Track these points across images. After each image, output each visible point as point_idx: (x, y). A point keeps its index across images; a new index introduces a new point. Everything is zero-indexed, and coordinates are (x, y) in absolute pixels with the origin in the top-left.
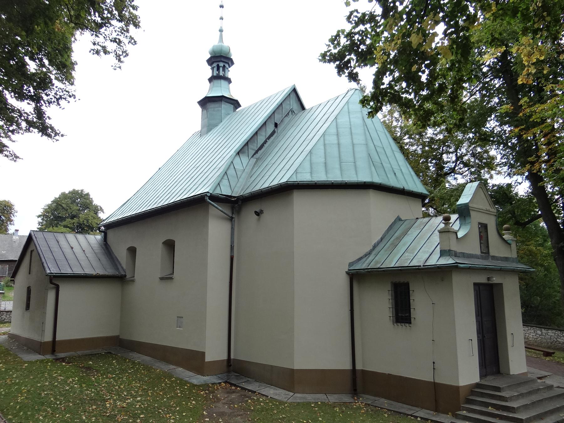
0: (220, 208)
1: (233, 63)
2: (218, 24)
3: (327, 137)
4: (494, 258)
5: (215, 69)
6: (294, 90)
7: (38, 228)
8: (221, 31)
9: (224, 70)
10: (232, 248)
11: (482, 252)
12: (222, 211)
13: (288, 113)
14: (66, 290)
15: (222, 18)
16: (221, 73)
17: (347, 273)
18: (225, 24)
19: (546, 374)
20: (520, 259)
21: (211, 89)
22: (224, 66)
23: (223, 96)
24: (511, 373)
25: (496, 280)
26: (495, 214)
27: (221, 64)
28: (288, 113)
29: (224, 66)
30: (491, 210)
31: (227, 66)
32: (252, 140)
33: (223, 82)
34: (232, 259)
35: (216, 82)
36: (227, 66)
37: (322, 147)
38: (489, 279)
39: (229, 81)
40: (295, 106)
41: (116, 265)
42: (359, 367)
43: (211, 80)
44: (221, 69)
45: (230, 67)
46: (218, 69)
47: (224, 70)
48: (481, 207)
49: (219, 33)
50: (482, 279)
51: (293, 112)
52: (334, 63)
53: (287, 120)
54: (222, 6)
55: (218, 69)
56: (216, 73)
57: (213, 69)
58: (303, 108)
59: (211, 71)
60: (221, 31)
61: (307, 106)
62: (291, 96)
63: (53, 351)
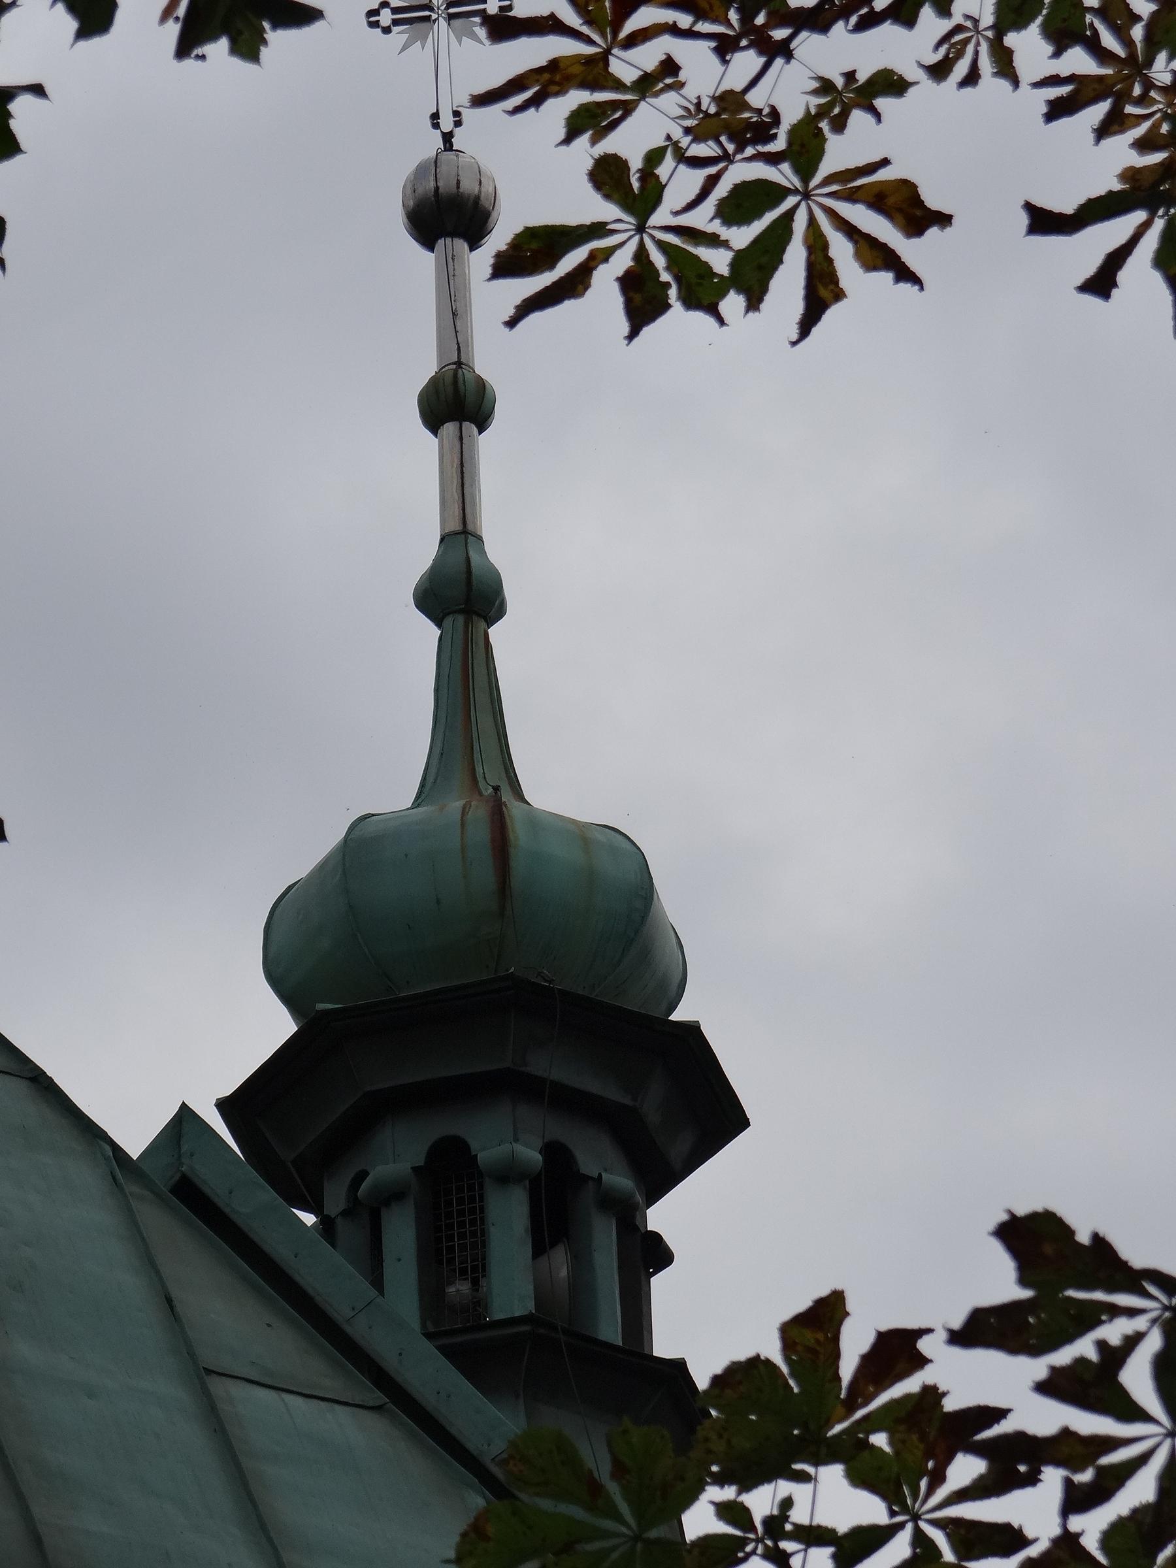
27: (506, 1140)
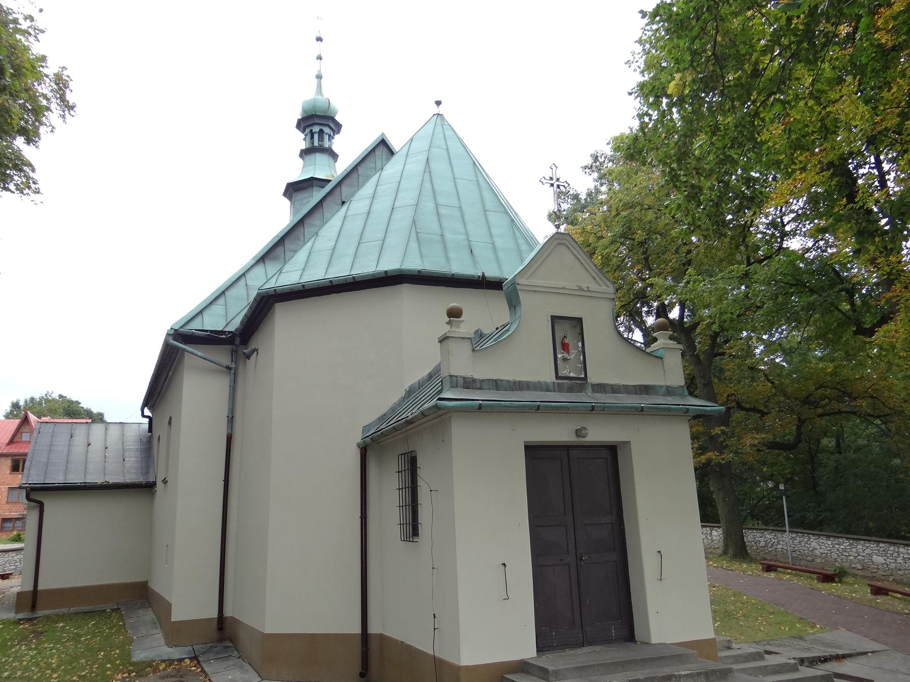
0: (199, 354)
2: (314, 67)
4: (600, 388)
8: (319, 77)
10: (231, 420)
11: (557, 377)
12: (205, 359)
14: (54, 508)
15: (319, 58)
16: (326, 144)
17: (358, 445)
18: (326, 68)
19: (869, 645)
20: (691, 387)
22: (321, 132)
24: (655, 640)
25: (600, 433)
26: (612, 296)
27: (316, 129)
29: (321, 132)
32: (293, 236)
34: (229, 439)
35: (310, 158)
38: (578, 433)
41: (148, 467)
42: (373, 629)
44: (316, 136)
48: (560, 284)
49: (316, 81)
50: (557, 432)
54: (319, 39)
60: (319, 77)
63: (34, 607)
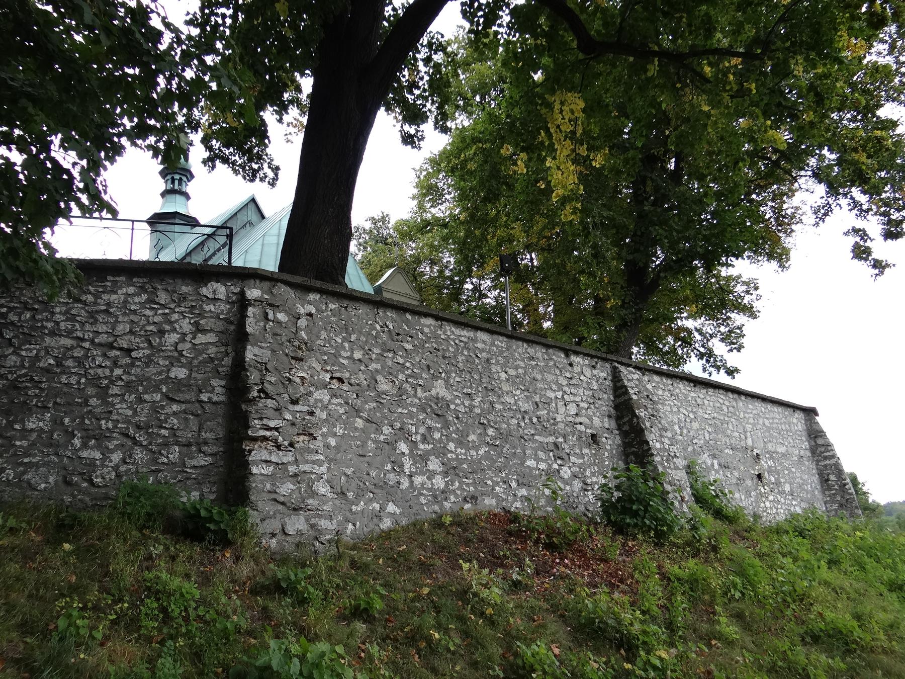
1: (192, 177)
3: (267, 238)
5: (169, 182)
6: (253, 200)
7: (162, 163)
9: (180, 184)
13: (245, 225)
16: (176, 187)
21: (163, 206)
23: (176, 213)
27: (177, 177)
28: (245, 225)
29: (181, 180)
30: (411, 294)
31: (184, 179)
33: (178, 198)
35: (170, 197)
36: (184, 179)
37: (260, 247)
39: (187, 196)
40: (254, 217)
43: (163, 195)
44: (176, 182)
45: (189, 181)
46: (173, 183)
47: (180, 184)
51: (251, 224)
52: (190, 176)
53: (243, 232)
55: (173, 183)
56: (170, 186)
57: (166, 182)
58: (263, 217)
59: (164, 185)
61: (266, 214)
62: (249, 206)
